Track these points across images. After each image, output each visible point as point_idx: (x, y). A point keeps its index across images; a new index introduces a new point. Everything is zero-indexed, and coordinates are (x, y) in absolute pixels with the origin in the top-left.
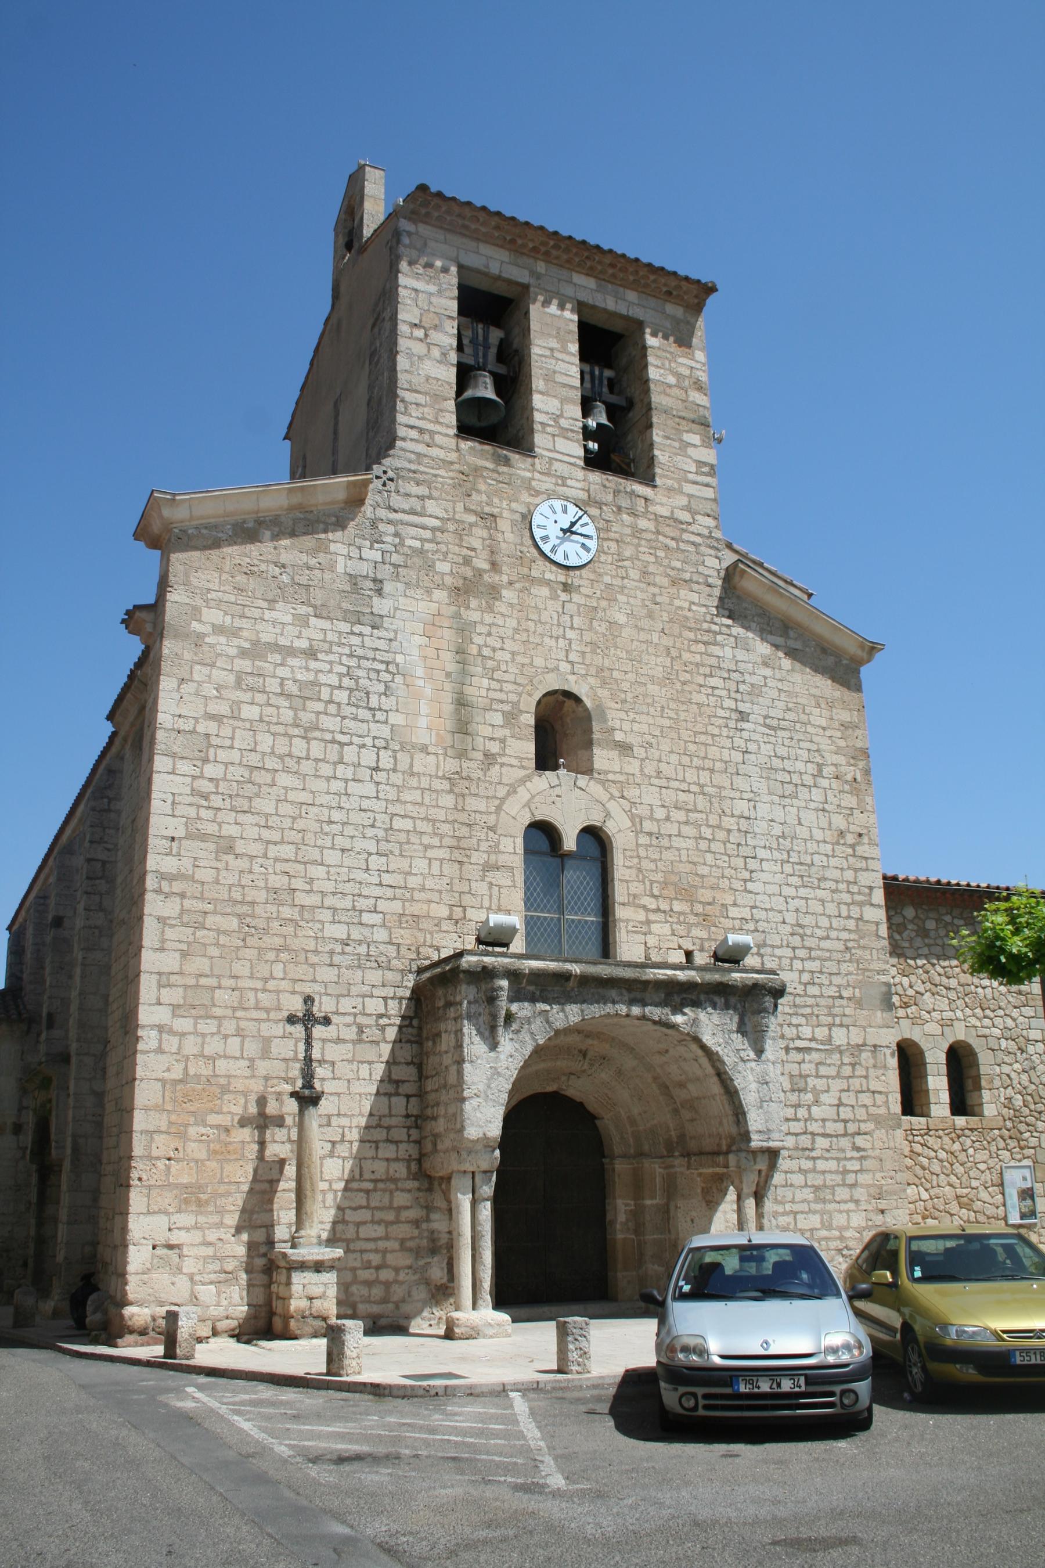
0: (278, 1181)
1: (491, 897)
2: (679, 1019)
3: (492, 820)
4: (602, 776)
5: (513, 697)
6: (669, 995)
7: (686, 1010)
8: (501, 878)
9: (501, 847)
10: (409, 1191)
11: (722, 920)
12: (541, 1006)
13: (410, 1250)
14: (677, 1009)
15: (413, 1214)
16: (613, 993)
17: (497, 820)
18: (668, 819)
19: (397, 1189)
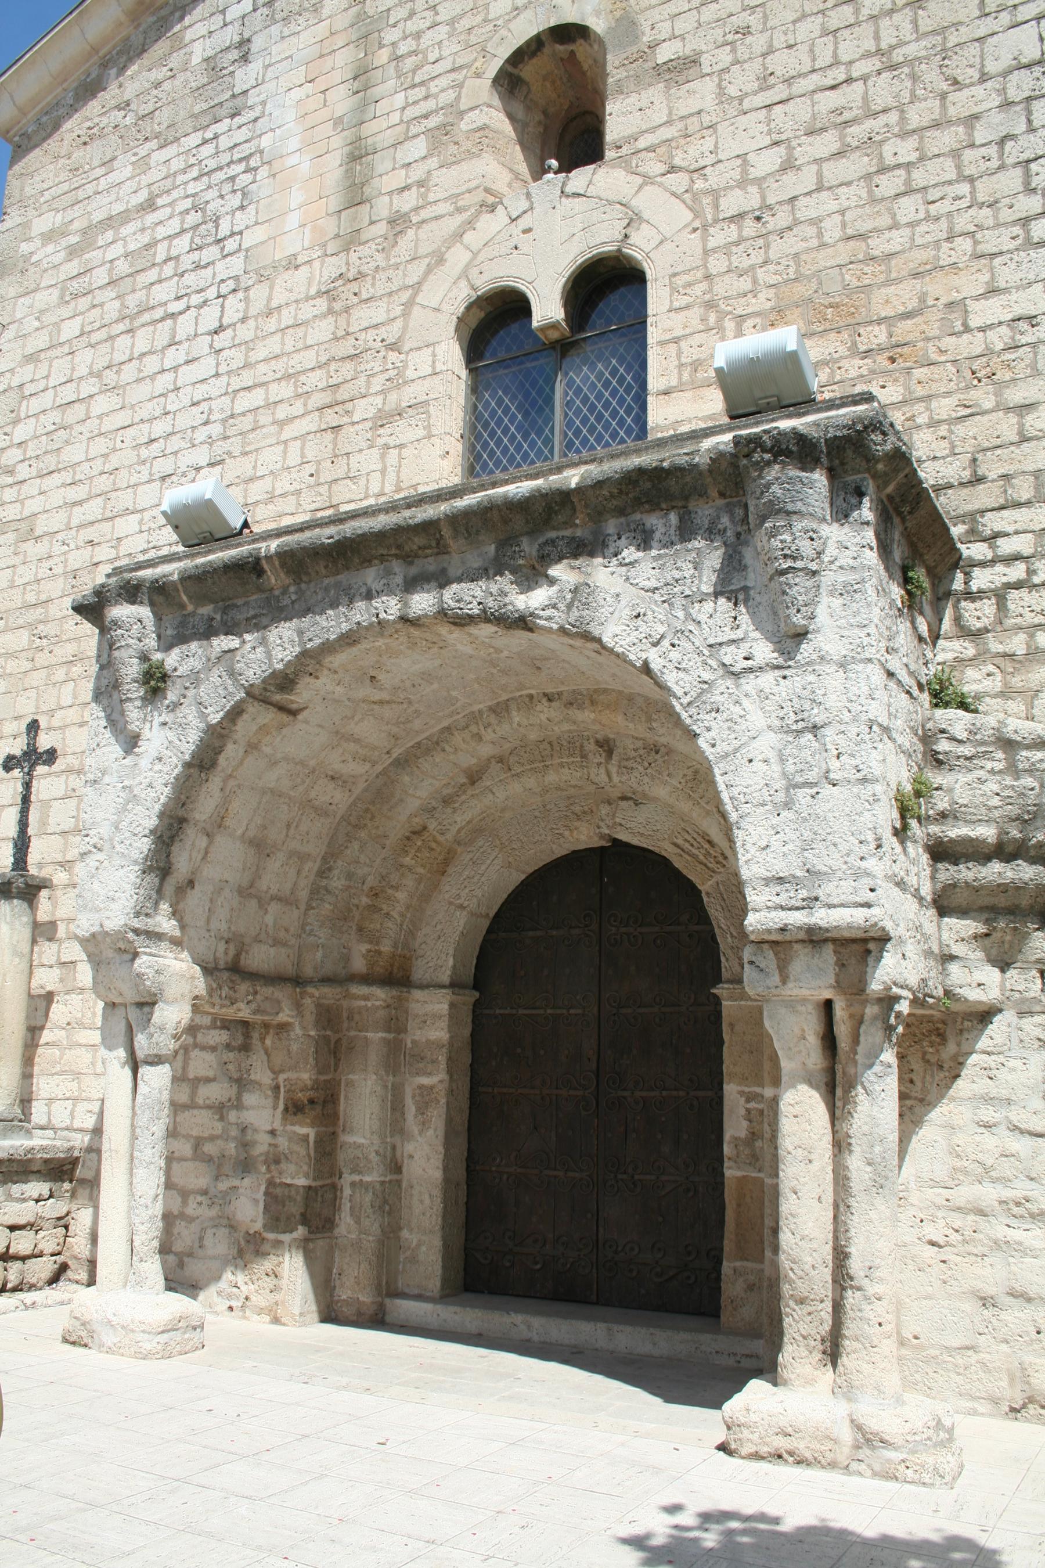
0: (42, 1028)
1: (383, 472)
2: (534, 600)
3: (391, 333)
4: (624, 151)
5: (450, 96)
6: (506, 542)
7: (554, 571)
8: (405, 431)
9: (410, 374)
10: (214, 1049)
11: (949, 342)
12: (223, 642)
13: (209, 1160)
14: (532, 576)
15: (216, 1092)
16: (370, 576)
17: (405, 329)
18: (788, 166)
19: (196, 1045)
